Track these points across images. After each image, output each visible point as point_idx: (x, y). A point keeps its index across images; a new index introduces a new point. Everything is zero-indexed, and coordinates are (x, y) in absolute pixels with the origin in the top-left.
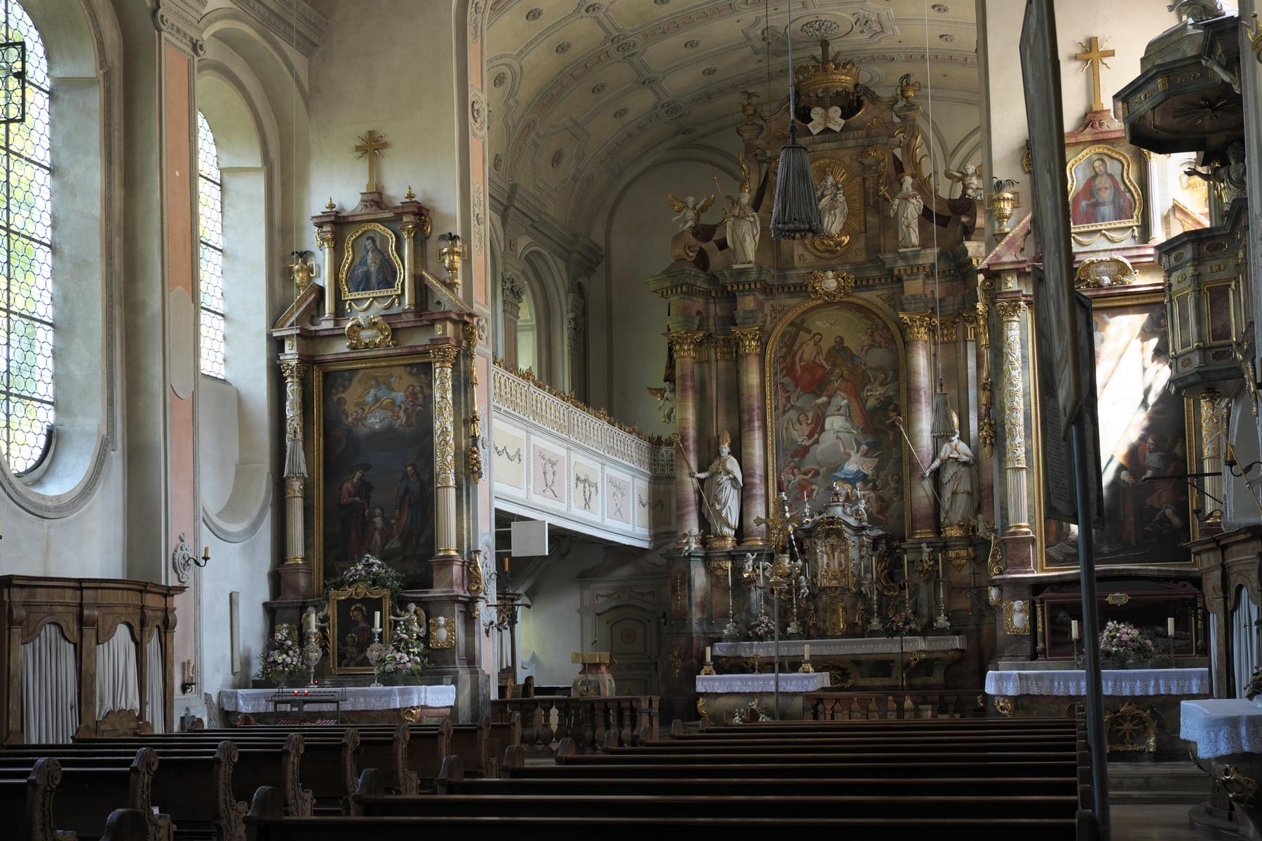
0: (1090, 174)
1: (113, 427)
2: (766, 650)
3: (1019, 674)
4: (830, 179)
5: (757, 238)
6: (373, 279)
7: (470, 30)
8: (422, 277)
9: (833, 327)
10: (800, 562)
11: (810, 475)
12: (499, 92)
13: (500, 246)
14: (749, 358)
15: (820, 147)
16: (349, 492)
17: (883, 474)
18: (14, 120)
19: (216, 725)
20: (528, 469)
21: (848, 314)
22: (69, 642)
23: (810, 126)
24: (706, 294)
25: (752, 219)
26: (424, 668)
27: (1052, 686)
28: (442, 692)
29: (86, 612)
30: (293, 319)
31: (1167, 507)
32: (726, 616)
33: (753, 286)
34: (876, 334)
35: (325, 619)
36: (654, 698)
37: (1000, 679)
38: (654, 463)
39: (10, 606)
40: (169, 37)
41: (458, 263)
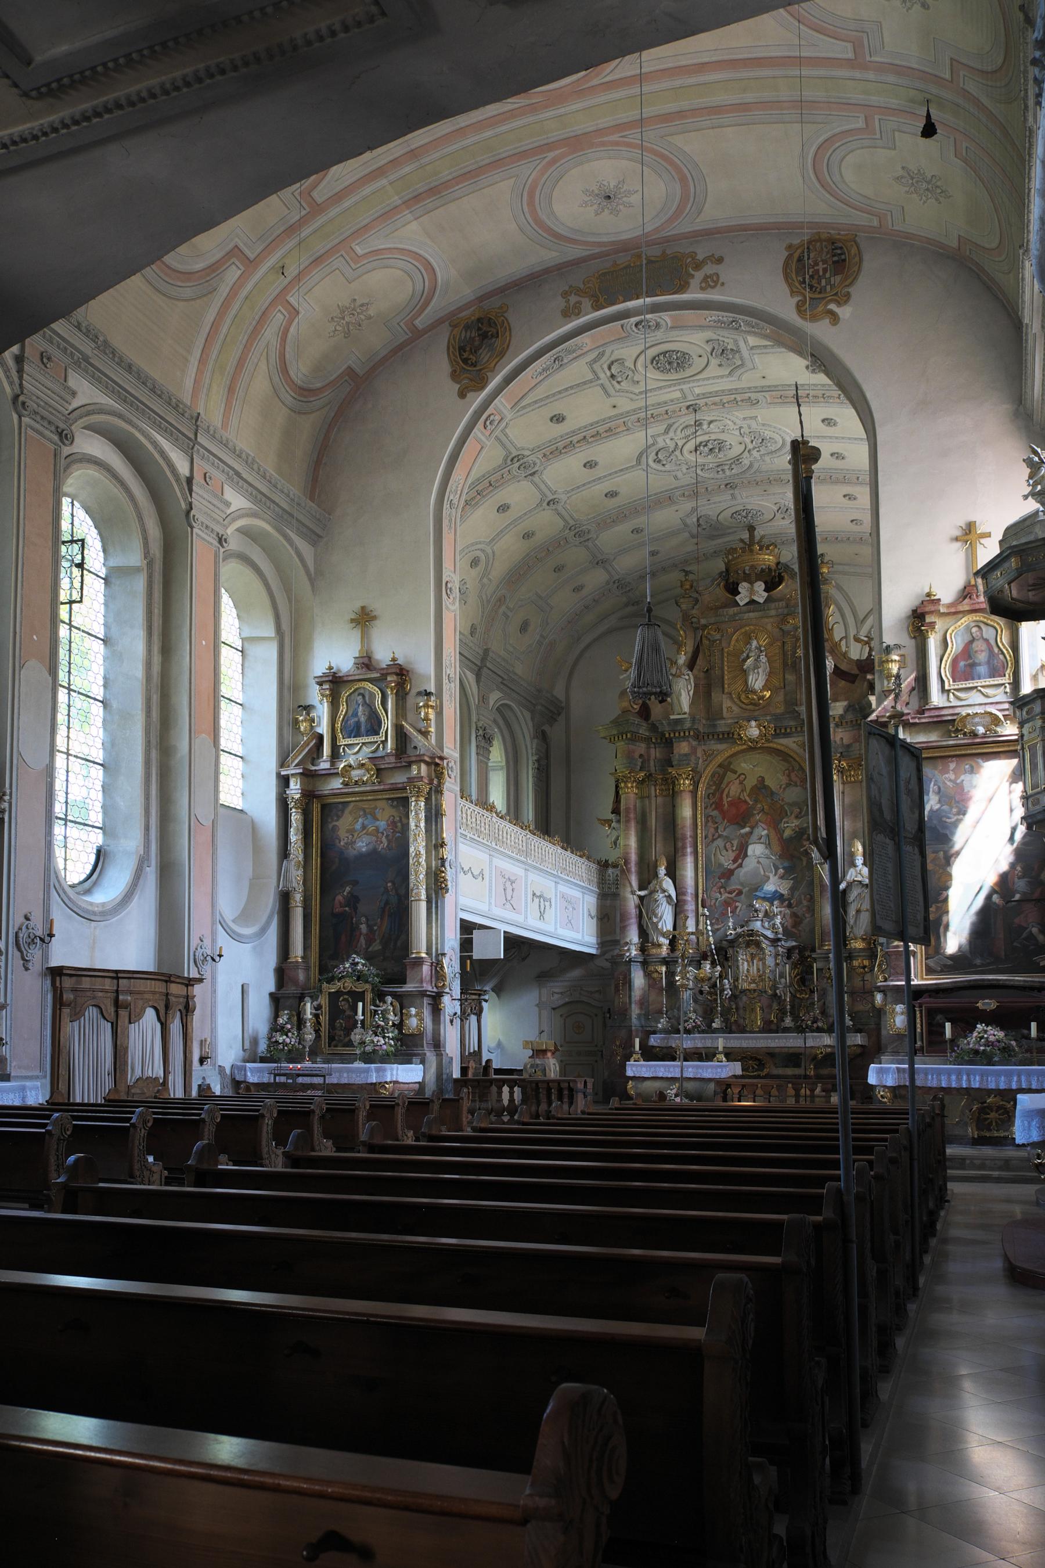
0: (968, 638)
1: (148, 847)
2: (693, 1042)
3: (898, 1068)
4: (754, 643)
5: (691, 693)
6: (363, 728)
7: (445, 523)
8: (402, 726)
9: (756, 769)
10: (719, 968)
11: (734, 894)
12: (474, 572)
13: (474, 700)
14: (683, 794)
15: (746, 616)
16: (340, 903)
17: (796, 894)
18: (75, 602)
19: (229, 1092)
20: (490, 886)
21: (768, 757)
22: (108, 1021)
23: (737, 598)
24: (648, 740)
25: (687, 677)
26: (397, 1050)
27: (926, 1079)
28: (412, 1070)
29: (121, 997)
30: (296, 761)
31: (1033, 926)
32: (660, 1012)
33: (687, 734)
34: (793, 775)
35: (318, 1008)
36: (588, 1080)
37: (880, 1071)
38: (602, 881)
39: (61, 991)
40: (200, 533)
41: (432, 715)
